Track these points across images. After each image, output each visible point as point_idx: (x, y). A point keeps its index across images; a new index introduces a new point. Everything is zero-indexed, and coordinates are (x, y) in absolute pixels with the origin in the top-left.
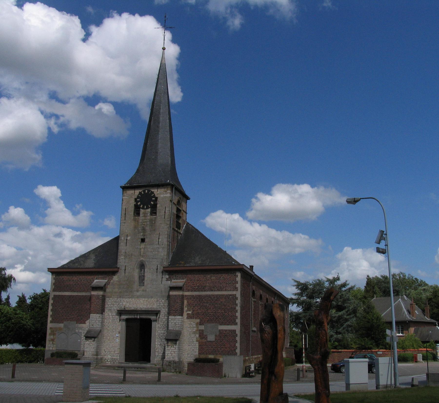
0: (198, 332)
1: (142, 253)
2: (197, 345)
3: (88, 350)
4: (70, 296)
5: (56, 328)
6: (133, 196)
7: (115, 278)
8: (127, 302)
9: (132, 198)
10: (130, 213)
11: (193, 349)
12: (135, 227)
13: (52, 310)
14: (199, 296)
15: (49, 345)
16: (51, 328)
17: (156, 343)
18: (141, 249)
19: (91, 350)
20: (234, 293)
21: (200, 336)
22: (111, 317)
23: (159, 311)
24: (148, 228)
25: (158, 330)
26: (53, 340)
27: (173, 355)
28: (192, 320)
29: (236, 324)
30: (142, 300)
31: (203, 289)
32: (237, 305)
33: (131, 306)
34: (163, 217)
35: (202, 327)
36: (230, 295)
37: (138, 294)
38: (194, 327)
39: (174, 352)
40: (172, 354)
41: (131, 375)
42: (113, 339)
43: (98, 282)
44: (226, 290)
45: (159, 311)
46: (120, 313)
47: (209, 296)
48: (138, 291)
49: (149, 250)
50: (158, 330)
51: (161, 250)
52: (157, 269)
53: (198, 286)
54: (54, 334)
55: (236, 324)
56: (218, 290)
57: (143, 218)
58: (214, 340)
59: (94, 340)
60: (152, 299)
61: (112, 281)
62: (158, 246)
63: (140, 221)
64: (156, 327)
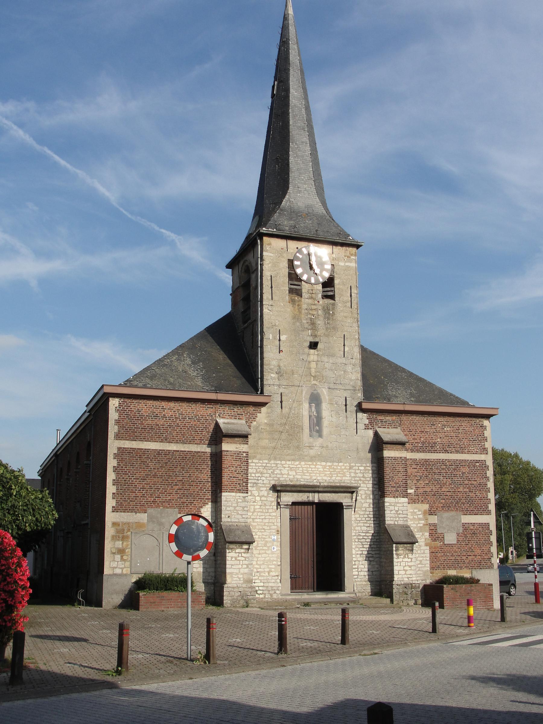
0: (427, 528)
1: (313, 370)
2: (428, 551)
3: (237, 571)
4: (159, 452)
5: (128, 523)
6: (285, 255)
7: (263, 416)
8: (291, 469)
9: (283, 257)
10: (282, 288)
11: (421, 561)
12: (296, 318)
13: (115, 482)
14: (426, 461)
15: (114, 564)
16: (114, 524)
17: (354, 552)
18: (309, 362)
19: (242, 571)
20: (482, 457)
21: (431, 535)
22: (258, 498)
23: (357, 488)
24: (320, 322)
25: (355, 525)
26: (121, 552)
27: (408, 573)
28: (416, 505)
29: (489, 513)
30: (320, 466)
31: (431, 448)
32: (488, 479)
33: (299, 477)
34: (349, 304)
35: (433, 519)
36: (477, 461)
37: (312, 452)
38: (420, 519)
39: (410, 566)
40: (406, 571)
41: (359, 618)
42: (265, 545)
43: (228, 423)
44: (469, 452)
45: (357, 488)
46: (277, 489)
47: (443, 462)
48: (311, 447)
49: (327, 365)
50: (355, 525)
51: (349, 368)
52: (346, 405)
53: (423, 443)
54: (124, 538)
55: (489, 513)
56: (457, 452)
57: (310, 301)
58: (455, 542)
59: (248, 549)
60: (341, 464)
61: (255, 423)
62: (344, 360)
63: (304, 306)
64: (351, 521)
